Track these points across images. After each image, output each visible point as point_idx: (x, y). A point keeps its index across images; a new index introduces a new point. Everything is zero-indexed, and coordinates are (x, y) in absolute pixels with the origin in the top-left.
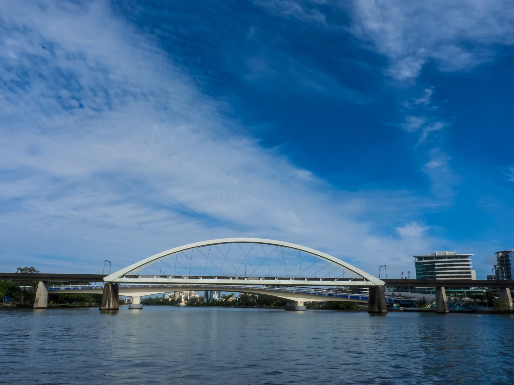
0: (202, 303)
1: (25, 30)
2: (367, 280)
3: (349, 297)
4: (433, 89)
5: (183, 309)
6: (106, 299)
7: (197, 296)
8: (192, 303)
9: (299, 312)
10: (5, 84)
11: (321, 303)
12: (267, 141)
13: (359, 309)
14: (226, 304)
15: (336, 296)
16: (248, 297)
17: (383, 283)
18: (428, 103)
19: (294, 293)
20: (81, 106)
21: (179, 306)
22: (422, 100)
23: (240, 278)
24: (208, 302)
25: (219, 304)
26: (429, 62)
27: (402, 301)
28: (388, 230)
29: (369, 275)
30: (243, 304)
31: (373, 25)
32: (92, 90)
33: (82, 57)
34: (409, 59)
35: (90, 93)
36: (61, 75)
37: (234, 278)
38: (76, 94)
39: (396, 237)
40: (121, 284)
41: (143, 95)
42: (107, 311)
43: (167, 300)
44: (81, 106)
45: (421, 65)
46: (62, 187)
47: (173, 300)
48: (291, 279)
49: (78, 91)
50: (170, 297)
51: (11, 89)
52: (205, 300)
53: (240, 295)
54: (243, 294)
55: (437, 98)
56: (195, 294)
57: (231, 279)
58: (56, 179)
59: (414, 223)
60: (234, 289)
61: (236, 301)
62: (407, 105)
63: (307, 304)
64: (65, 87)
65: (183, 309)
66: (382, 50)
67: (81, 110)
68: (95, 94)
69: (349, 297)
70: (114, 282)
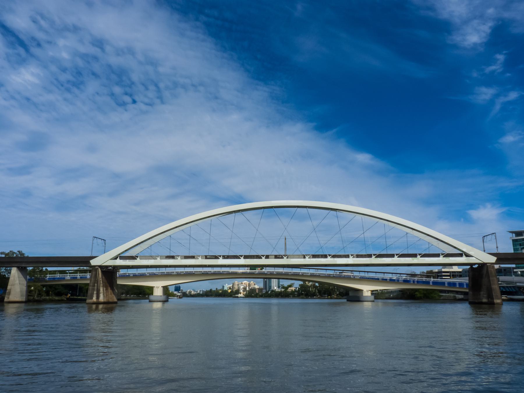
0: (260, 294)
1: (75, 29)
2: (467, 255)
3: (431, 284)
4: (505, 54)
5: (241, 301)
6: (94, 290)
7: (257, 287)
8: (251, 294)
9: (366, 304)
10: (62, 85)
11: (392, 292)
12: (322, 125)
13: (442, 298)
14: (284, 294)
16: (309, 287)
17: (493, 259)
18: (500, 70)
20: (134, 102)
21: (238, 297)
22: (493, 68)
23: (276, 257)
24: (267, 292)
26: (500, 23)
28: (458, 213)
29: (470, 247)
30: (302, 294)
32: (143, 85)
33: (130, 51)
34: (475, 22)
35: (142, 88)
37: (267, 257)
38: (128, 90)
39: (468, 220)
40: (122, 272)
41: (193, 85)
42: (94, 306)
43: (226, 291)
44: (134, 102)
45: (490, 27)
46: (122, 183)
49: (130, 87)
50: (230, 289)
51: (68, 90)
53: (300, 285)
54: (301, 283)
55: (509, 64)
56: (255, 284)
57: (264, 258)
58: (116, 176)
59: (489, 205)
60: (294, 277)
61: (295, 291)
64: (117, 84)
65: (241, 301)
66: (444, 15)
67: (134, 106)
68: (147, 89)
69: (431, 284)
70: (110, 266)
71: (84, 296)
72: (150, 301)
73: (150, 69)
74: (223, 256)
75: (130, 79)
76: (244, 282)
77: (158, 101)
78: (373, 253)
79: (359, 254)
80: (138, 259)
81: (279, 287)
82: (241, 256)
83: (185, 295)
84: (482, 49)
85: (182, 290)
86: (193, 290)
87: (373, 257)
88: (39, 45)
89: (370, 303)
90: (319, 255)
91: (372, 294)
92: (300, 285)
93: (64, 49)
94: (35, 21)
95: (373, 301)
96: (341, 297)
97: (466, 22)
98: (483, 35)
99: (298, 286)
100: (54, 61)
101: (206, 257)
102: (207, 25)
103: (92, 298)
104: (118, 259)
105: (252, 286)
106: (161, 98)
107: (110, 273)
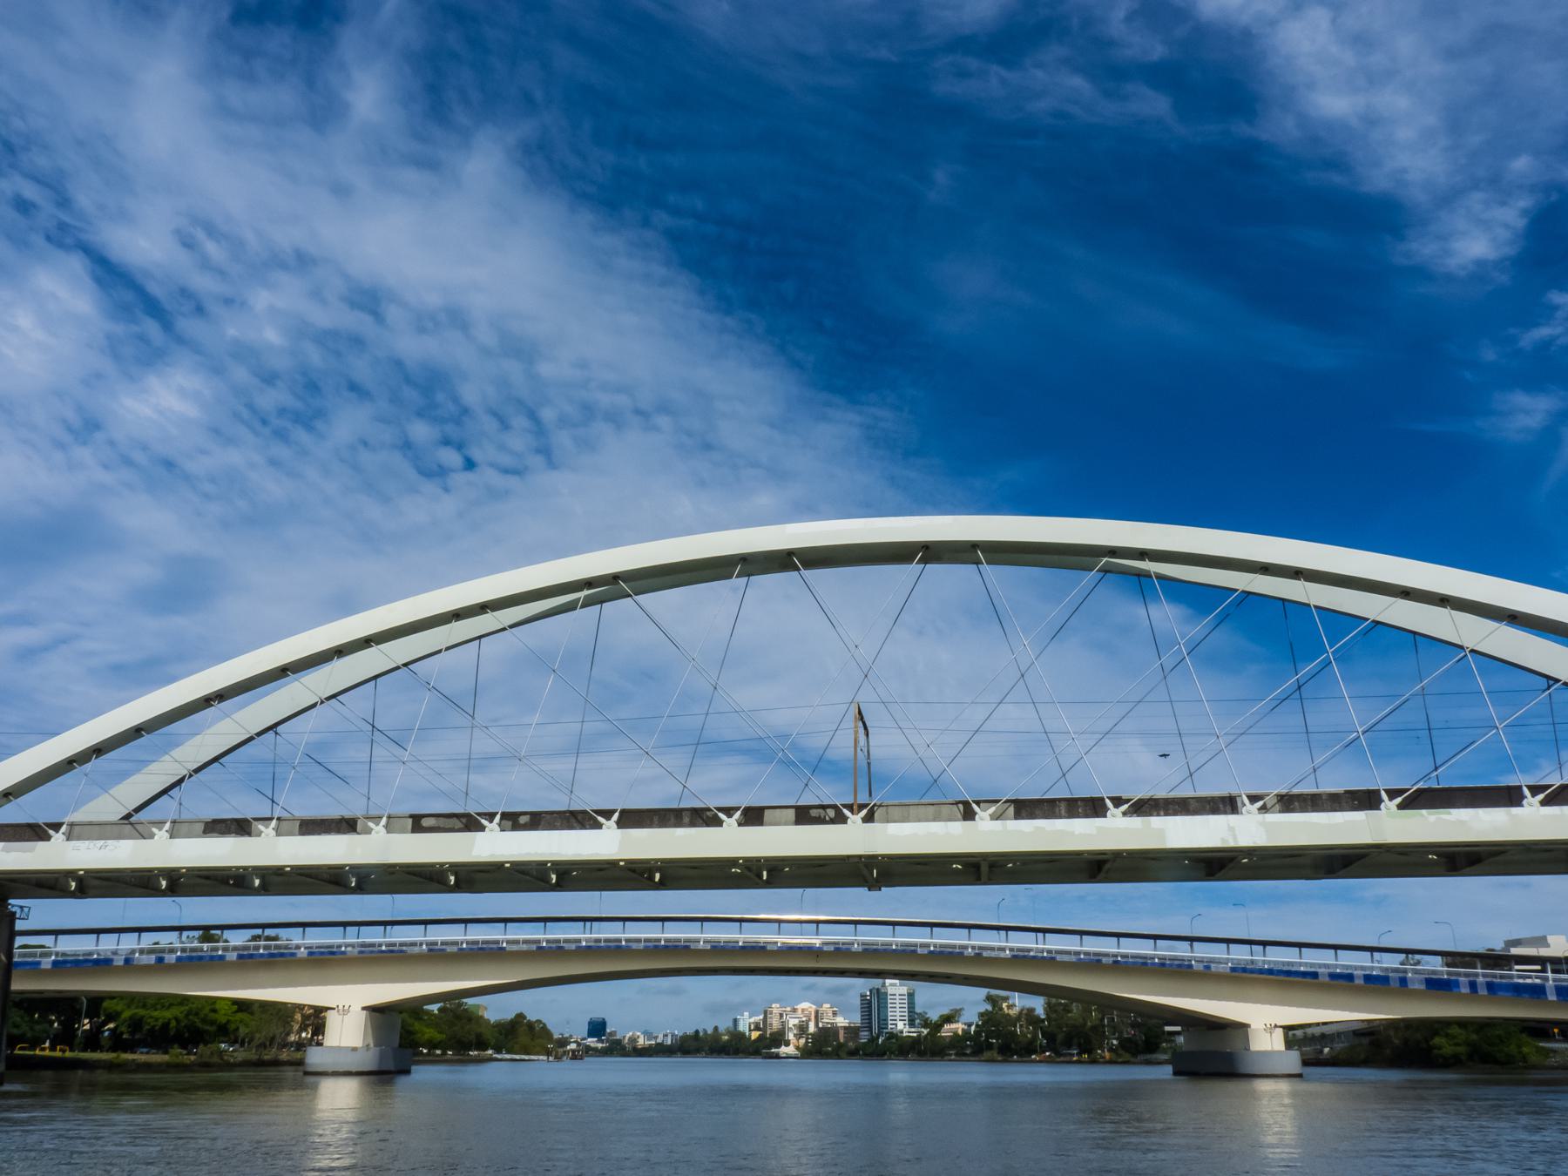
1: (302, 262)
7: (841, 1021)
8: (823, 1046)
9: (1264, 1086)
10: (264, 422)
14: (928, 1046)
15: (1473, 985)
19: (1219, 978)
20: (470, 465)
21: (777, 1056)
22: (1543, 332)
24: (873, 1040)
26: (1554, 197)
30: (990, 1047)
31: (1333, 104)
32: (495, 414)
33: (457, 319)
34: (1476, 199)
35: (490, 425)
36: (408, 380)
37: (753, 816)
38: (450, 429)
41: (638, 412)
44: (470, 465)
45: (1524, 212)
47: (760, 1038)
49: (458, 422)
51: (281, 435)
52: (864, 1037)
56: (835, 1014)
62: (1489, 354)
63: (1311, 1040)
64: (420, 414)
65: (790, 1072)
66: (1377, 181)
67: (469, 476)
68: (505, 425)
72: (307, 1073)
73: (514, 370)
74: (505, 816)
75: (456, 400)
76: (800, 1006)
77: (537, 461)
79: (1296, 791)
81: (911, 1023)
83: (617, 1049)
84: (1503, 279)
86: (645, 1033)
87: (1389, 806)
88: (200, 310)
89: (1283, 1086)
90: (1053, 802)
91: (1290, 1044)
92: (981, 1015)
93: (268, 318)
94: (188, 244)
95: (1300, 1076)
96: (1127, 1057)
97: (1448, 199)
98: (1504, 234)
99: (975, 1019)
100: (244, 353)
102: (675, 238)
105: (827, 1020)
106: (545, 452)
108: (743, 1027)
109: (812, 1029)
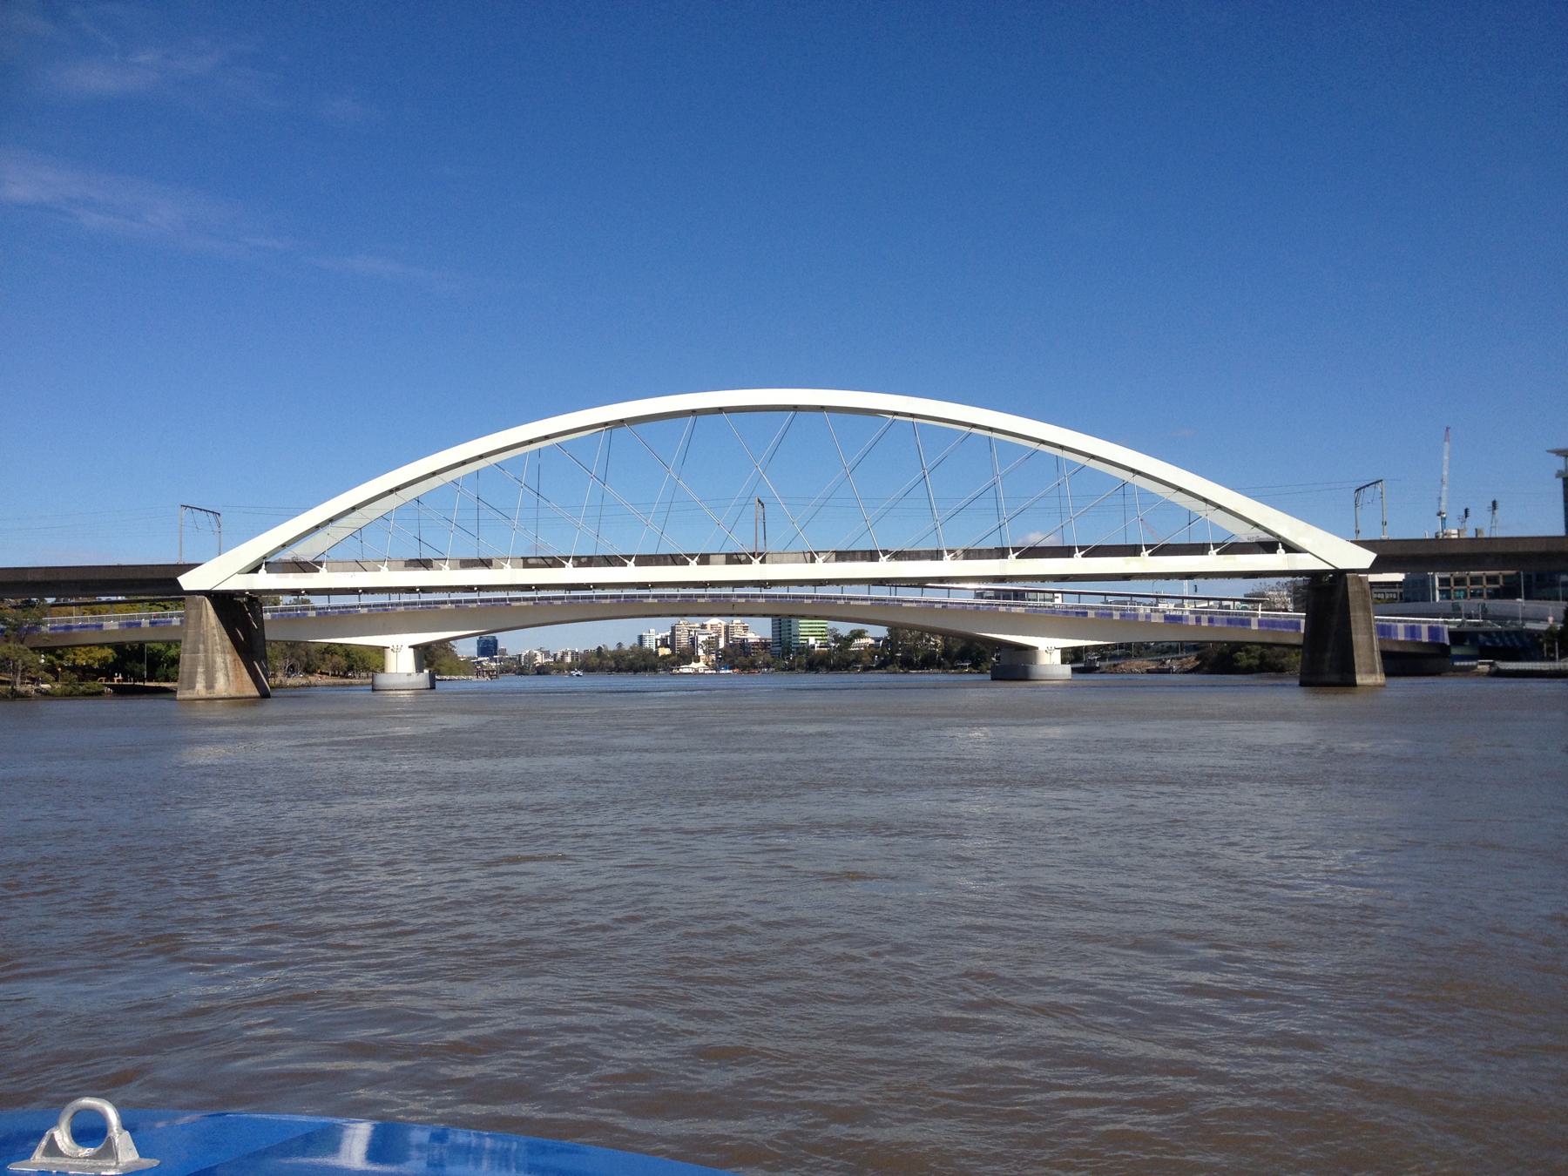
2: (1291, 548)
7: (752, 637)
8: (737, 656)
14: (838, 659)
17: (1365, 558)
23: (732, 559)
25: (815, 663)
27: (1487, 634)
37: (704, 560)
48: (947, 557)
56: (746, 629)
71: (167, 680)
78: (1009, 544)
80: (323, 570)
82: (629, 557)
85: (504, 652)
101: (527, 563)
103: (192, 687)
104: (262, 571)
105: (738, 634)
107: (235, 609)
108: (650, 643)
109: (722, 645)
